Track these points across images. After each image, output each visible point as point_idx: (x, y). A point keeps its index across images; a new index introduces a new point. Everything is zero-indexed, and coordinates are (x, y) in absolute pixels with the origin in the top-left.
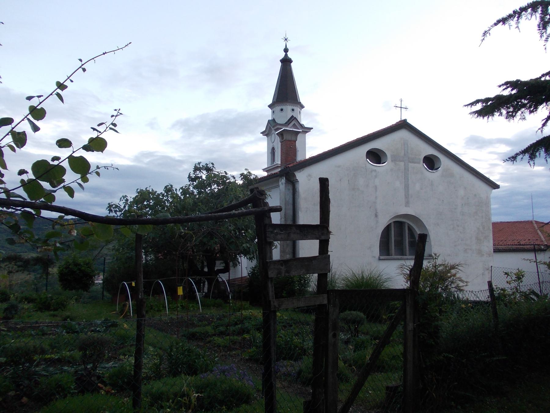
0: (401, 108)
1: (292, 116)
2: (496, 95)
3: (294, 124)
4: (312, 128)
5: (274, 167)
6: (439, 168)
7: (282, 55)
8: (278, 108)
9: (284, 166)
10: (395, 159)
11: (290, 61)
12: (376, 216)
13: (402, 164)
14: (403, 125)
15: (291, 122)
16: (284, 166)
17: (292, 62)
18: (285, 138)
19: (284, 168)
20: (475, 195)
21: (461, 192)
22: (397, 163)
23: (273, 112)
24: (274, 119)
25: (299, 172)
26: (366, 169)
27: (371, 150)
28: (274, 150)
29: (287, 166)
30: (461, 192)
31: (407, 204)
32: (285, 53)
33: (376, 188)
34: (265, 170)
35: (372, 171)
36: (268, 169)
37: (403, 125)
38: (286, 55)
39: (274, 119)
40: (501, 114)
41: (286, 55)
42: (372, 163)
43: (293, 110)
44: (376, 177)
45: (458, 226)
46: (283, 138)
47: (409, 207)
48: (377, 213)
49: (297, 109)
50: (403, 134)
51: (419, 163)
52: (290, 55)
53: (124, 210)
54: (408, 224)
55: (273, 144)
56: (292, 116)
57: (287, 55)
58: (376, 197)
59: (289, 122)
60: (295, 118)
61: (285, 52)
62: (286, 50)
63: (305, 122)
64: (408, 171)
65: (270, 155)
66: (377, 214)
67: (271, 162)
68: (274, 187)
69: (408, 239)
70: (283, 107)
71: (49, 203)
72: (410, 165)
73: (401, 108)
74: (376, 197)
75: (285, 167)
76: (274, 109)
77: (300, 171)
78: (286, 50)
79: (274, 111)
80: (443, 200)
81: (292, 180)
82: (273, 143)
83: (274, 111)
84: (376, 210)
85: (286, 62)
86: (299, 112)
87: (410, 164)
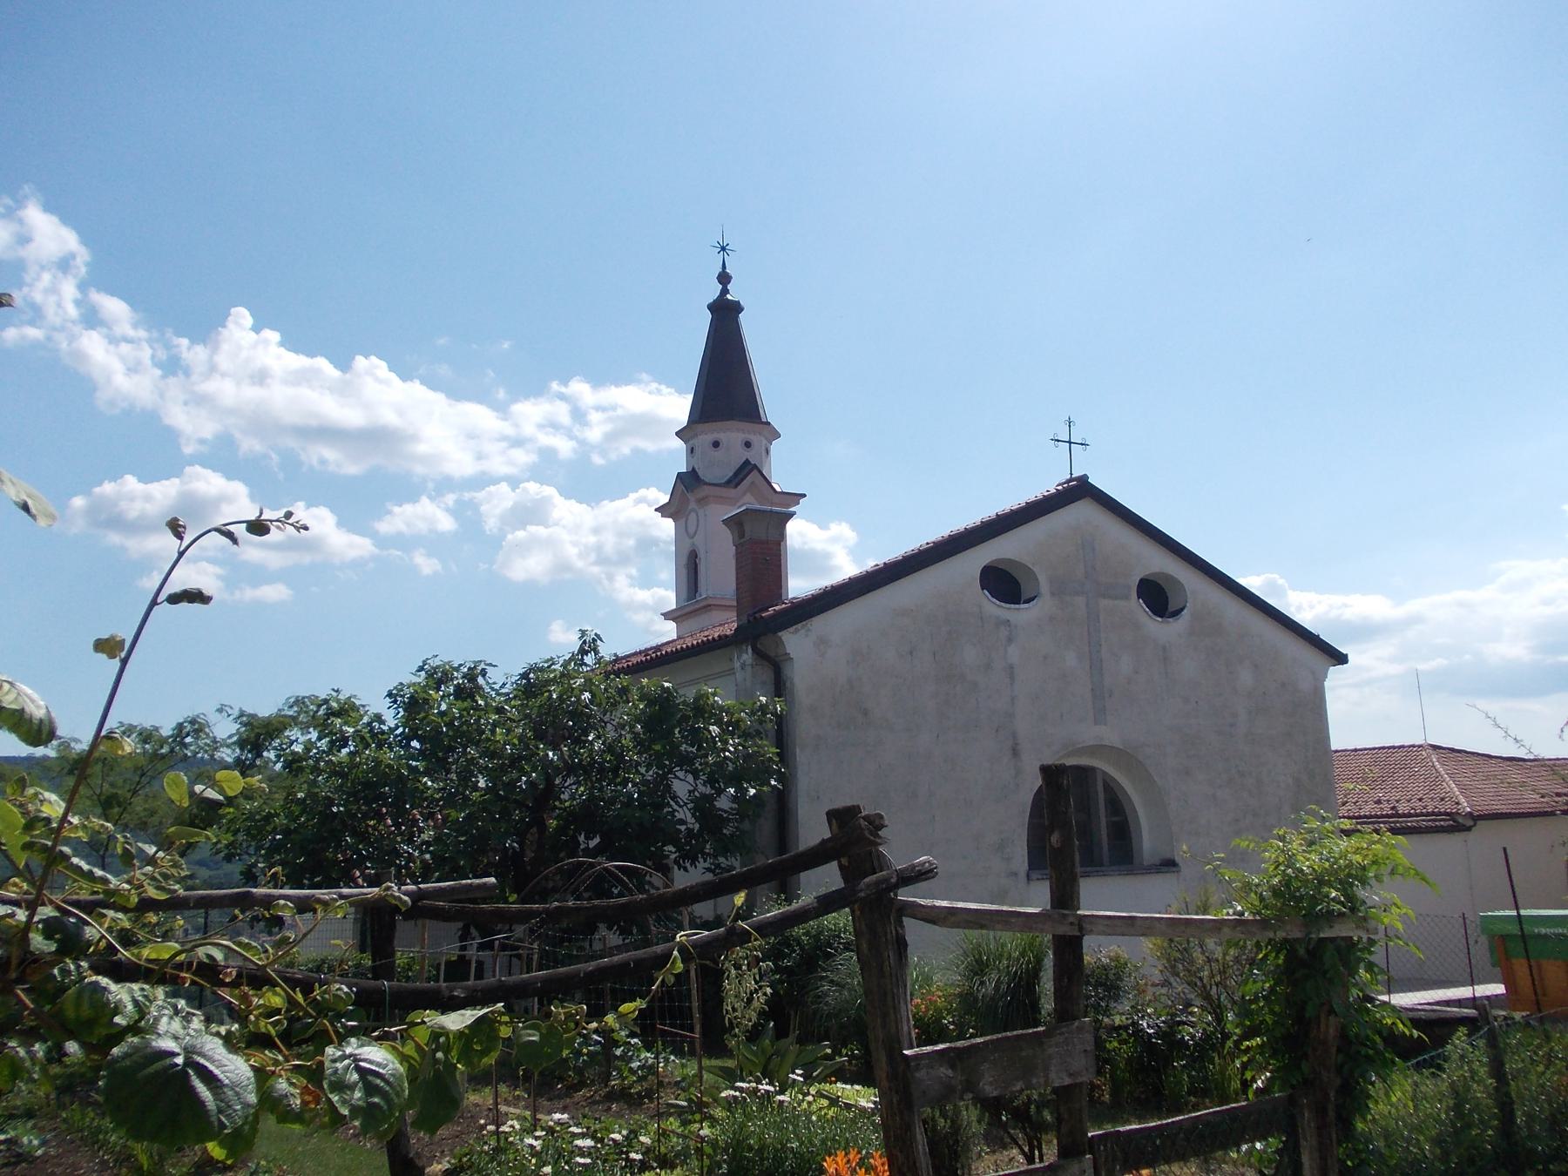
0: (1070, 442)
1: (747, 462)
4: (804, 496)
5: (697, 606)
6: (1182, 609)
8: (705, 438)
9: (749, 615)
10: (1061, 589)
11: (736, 308)
12: (1015, 752)
13: (1080, 601)
14: (1079, 490)
15: (742, 480)
16: (749, 615)
17: (742, 310)
18: (747, 537)
19: (749, 621)
21: (1246, 677)
23: (692, 450)
24: (693, 469)
26: (981, 618)
27: (995, 565)
28: (696, 557)
29: (757, 615)
31: (1100, 716)
33: (1011, 671)
34: (671, 617)
36: (679, 613)
37: (1079, 490)
39: (693, 469)
43: (748, 445)
44: (1010, 640)
46: (742, 534)
47: (1105, 725)
50: (1083, 510)
51: (1127, 597)
53: (693, 974)
55: (691, 540)
56: (747, 462)
58: (1013, 699)
59: (737, 480)
60: (755, 467)
62: (724, 278)
63: (781, 480)
64: (1099, 622)
65: (684, 571)
67: (689, 592)
68: (724, 671)
69: (1106, 817)
70: (721, 436)
71: (316, 880)
72: (1104, 603)
73: (1070, 442)
74: (1013, 699)
75: (751, 619)
76: (695, 442)
77: (797, 631)
78: (724, 278)
79: (693, 448)
80: (1197, 702)
81: (772, 654)
82: (693, 537)
83: (693, 448)
84: (1014, 735)
85: (725, 314)
86: (764, 453)
87: (1104, 603)
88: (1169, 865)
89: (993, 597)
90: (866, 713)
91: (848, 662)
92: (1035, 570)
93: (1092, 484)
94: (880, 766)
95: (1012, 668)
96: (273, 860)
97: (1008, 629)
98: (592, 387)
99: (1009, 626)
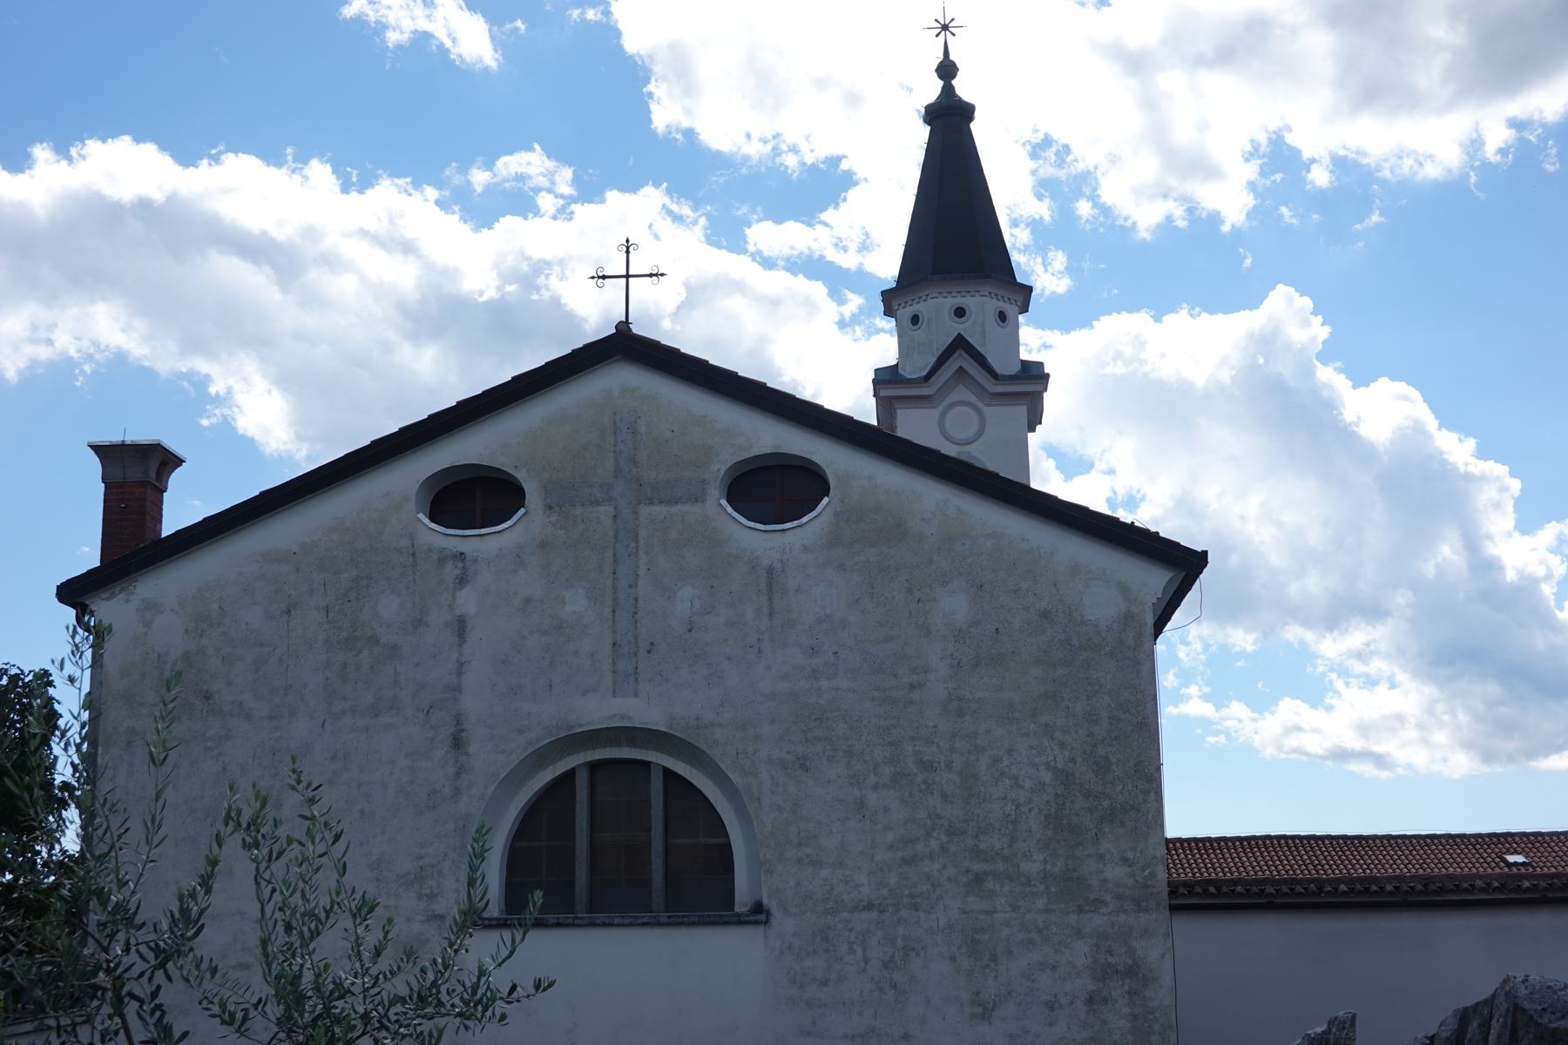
2: (176, 165)
3: (961, 369)
7: (932, 89)
11: (965, 112)
12: (458, 743)
20: (1045, 615)
22: (578, 511)
25: (107, 599)
30: (956, 606)
32: (941, 83)
35: (441, 561)
38: (948, 90)
40: (1092, 208)
41: (948, 90)
42: (509, 523)
44: (462, 581)
45: (928, 767)
48: (463, 730)
49: (982, 303)
50: (622, 378)
51: (698, 499)
52: (963, 88)
54: (668, 774)
57: (953, 88)
58: (461, 664)
61: (941, 77)
62: (947, 70)
66: (464, 734)
74: (461, 664)
77: (113, 595)
78: (947, 70)
84: (458, 720)
88: (759, 914)
89: (813, 509)
90: (208, 697)
91: (187, 631)
92: (518, 476)
93: (638, 335)
94: (224, 769)
95: (464, 621)
96: (72, 919)
97: (460, 565)
98: (825, 257)
99: (463, 561)
